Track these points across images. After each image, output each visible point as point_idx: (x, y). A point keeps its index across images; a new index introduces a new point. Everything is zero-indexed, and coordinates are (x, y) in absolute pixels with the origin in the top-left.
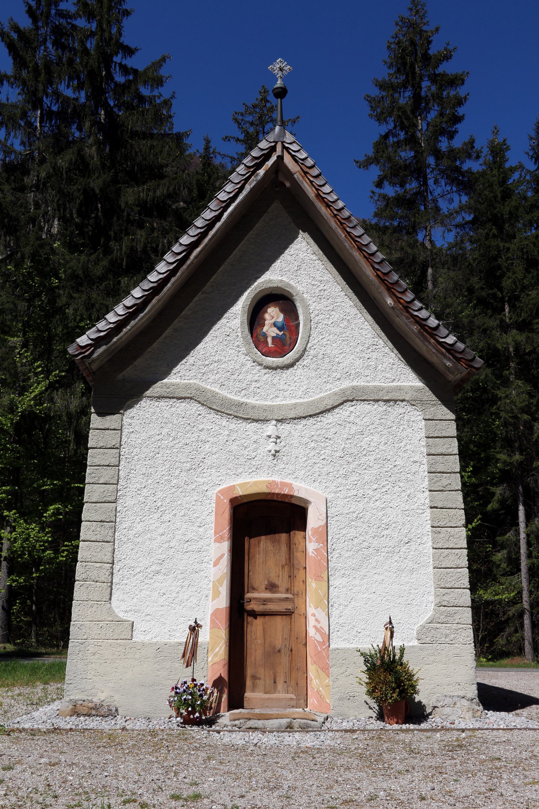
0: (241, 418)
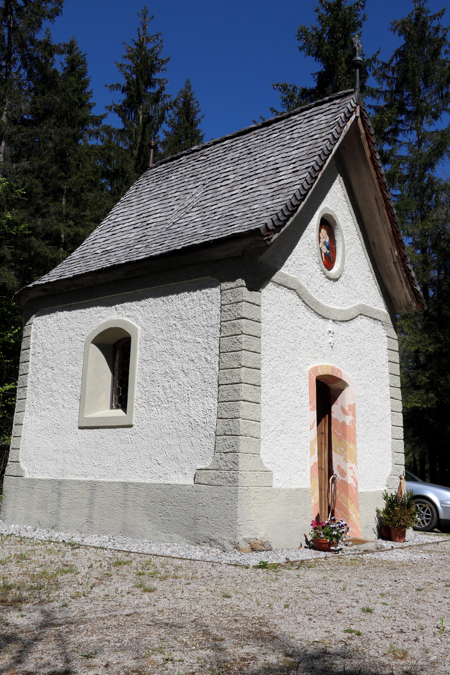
0: (317, 313)
